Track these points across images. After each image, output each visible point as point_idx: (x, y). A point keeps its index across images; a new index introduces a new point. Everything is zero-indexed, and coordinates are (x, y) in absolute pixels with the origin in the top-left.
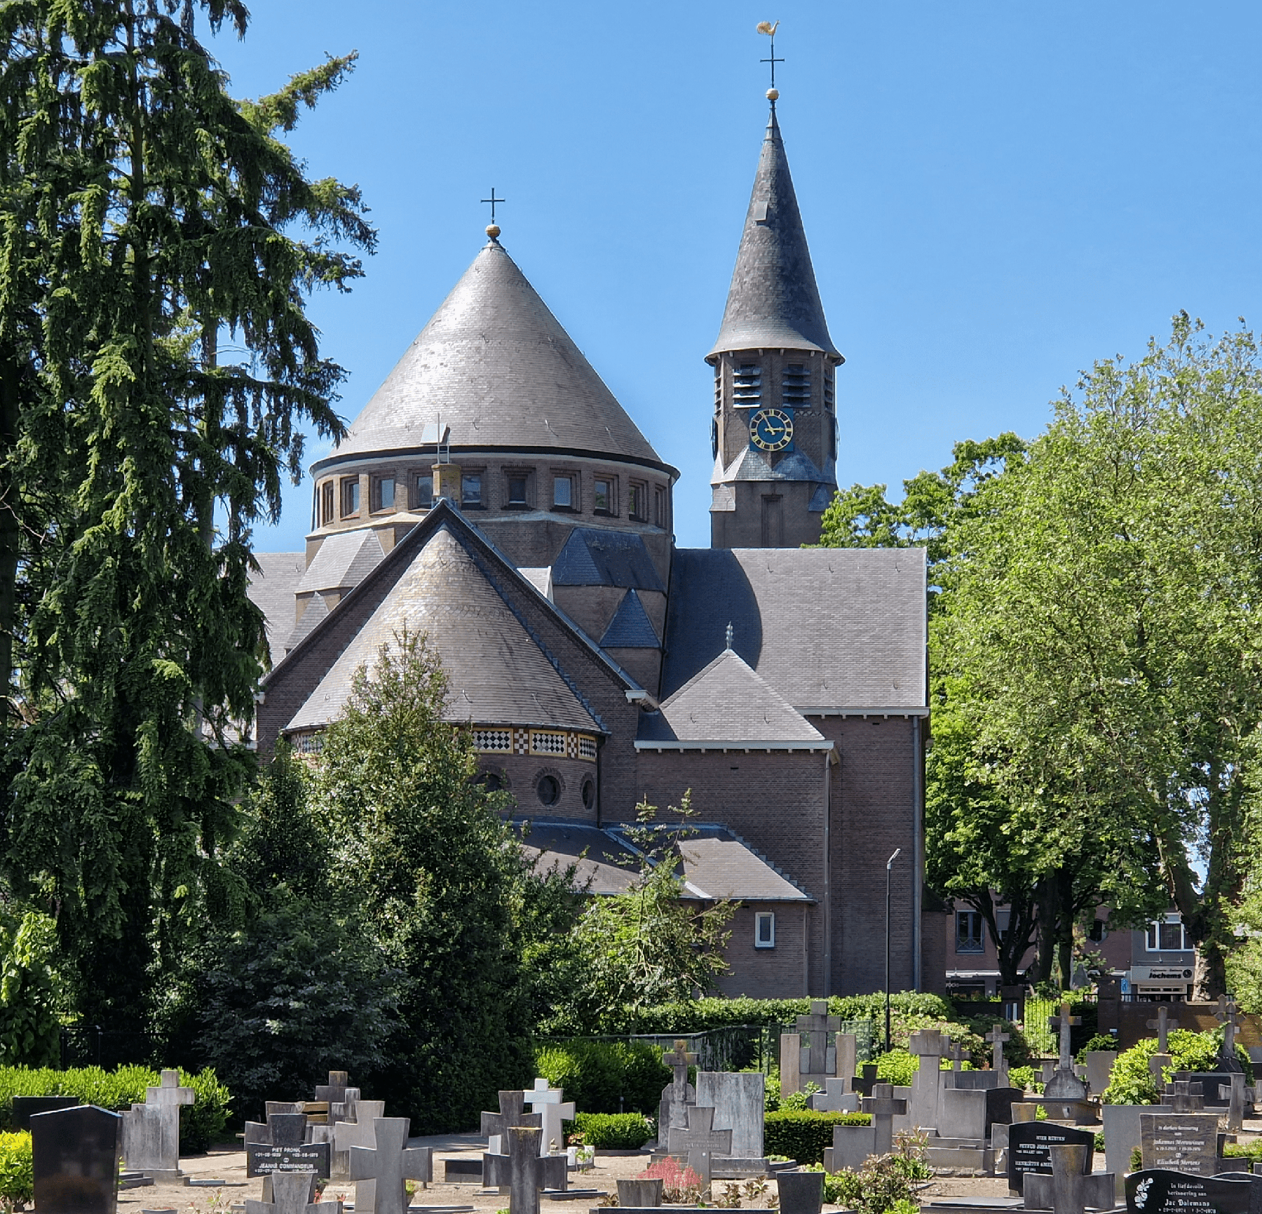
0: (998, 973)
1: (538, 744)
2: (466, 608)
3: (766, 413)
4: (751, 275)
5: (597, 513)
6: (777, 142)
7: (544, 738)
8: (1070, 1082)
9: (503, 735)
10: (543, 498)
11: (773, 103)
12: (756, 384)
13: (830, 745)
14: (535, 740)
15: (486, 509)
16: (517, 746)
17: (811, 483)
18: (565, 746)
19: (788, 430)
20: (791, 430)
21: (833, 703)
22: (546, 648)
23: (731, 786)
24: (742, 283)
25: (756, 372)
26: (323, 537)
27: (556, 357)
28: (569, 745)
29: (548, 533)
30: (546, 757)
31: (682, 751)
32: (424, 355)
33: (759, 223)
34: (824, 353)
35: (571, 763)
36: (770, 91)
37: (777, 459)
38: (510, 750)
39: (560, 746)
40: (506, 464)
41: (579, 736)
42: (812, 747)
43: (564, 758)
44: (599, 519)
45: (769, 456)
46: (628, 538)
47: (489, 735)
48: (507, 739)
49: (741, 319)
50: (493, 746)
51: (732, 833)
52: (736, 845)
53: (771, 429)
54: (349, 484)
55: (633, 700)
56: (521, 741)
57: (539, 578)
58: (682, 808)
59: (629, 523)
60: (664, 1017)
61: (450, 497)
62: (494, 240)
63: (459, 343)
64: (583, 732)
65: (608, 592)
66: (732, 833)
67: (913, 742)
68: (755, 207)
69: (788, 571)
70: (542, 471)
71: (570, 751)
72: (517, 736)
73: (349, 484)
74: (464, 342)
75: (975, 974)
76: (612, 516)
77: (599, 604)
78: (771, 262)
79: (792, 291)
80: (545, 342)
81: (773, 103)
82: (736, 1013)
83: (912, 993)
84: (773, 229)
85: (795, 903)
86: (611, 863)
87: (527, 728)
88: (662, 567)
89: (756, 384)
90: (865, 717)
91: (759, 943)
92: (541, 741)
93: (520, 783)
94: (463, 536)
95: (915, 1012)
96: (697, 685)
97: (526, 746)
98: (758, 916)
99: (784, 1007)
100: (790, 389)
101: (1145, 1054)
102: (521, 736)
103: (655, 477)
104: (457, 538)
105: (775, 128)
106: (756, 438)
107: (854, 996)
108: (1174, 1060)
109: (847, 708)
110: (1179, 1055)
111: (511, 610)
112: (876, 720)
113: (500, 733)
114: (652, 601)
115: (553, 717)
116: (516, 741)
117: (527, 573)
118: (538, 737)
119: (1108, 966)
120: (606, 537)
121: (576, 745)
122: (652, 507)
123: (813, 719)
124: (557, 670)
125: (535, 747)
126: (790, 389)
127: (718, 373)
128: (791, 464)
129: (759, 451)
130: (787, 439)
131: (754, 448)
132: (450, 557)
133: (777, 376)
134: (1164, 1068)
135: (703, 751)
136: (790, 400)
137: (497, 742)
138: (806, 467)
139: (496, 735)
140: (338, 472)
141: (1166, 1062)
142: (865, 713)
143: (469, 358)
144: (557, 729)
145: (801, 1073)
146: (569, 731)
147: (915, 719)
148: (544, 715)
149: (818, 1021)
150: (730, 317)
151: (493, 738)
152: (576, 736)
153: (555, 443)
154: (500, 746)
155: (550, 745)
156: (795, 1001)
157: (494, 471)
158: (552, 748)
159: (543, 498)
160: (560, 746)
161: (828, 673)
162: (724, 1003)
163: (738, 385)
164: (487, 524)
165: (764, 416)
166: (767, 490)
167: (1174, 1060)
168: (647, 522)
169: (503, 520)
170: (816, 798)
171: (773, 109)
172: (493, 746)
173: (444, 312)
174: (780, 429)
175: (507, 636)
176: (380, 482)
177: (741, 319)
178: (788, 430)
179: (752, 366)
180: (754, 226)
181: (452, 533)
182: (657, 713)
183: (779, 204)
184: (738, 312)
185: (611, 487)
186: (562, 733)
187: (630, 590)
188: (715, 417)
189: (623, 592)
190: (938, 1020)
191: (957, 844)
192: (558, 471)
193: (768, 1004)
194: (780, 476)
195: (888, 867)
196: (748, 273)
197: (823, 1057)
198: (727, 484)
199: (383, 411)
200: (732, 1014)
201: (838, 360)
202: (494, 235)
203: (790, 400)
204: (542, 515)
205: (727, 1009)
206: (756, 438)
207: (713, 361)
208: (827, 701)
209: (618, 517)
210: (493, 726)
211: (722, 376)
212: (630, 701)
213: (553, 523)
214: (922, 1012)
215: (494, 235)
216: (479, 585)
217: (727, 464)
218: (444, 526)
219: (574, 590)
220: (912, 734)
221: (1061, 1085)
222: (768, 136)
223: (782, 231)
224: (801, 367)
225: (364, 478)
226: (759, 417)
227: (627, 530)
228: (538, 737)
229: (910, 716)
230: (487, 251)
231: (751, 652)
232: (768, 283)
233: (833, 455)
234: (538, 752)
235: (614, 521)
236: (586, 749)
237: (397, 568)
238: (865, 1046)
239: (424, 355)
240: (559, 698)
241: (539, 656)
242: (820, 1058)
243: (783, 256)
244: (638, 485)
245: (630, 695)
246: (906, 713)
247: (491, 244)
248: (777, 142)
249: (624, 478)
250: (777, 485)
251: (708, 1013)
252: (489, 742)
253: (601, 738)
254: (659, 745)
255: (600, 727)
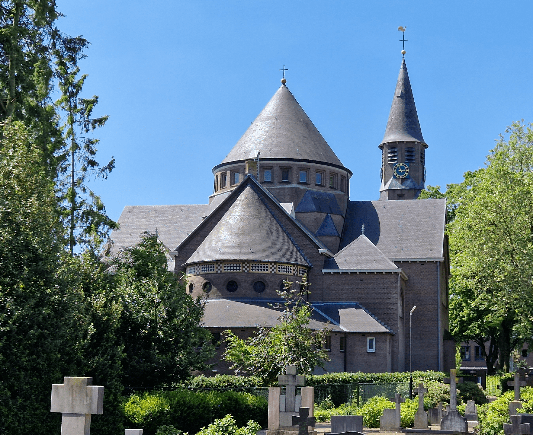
0: (486, 368)
1: (280, 269)
2: (255, 216)
3: (399, 164)
4: (395, 116)
5: (317, 185)
6: (405, 69)
7: (283, 267)
8: (457, 419)
9: (266, 266)
10: (295, 179)
11: (404, 55)
12: (396, 154)
13: (400, 270)
14: (279, 268)
15: (273, 183)
16: (271, 270)
17: (415, 189)
18: (292, 271)
19: (407, 170)
20: (408, 170)
21: (405, 257)
22: (288, 233)
23: (360, 287)
24: (392, 119)
25: (396, 150)
26: (214, 196)
27: (304, 127)
28: (294, 270)
29: (296, 192)
30: (284, 275)
31: (341, 273)
32: (254, 127)
33: (398, 97)
34: (420, 143)
35: (295, 277)
36: (402, 51)
37: (403, 181)
38: (268, 272)
39: (290, 270)
40: (281, 166)
41: (298, 267)
42: (393, 271)
43: (291, 276)
44: (317, 187)
45: (400, 180)
46: (329, 195)
47: (260, 266)
48: (267, 267)
49: (391, 131)
50: (261, 270)
51: (361, 306)
52: (362, 311)
53: (401, 170)
54: (224, 176)
55: (322, 253)
56: (273, 268)
57: (288, 208)
58: (303, 282)
59: (329, 189)
60: (323, 380)
61: (252, 174)
62: (284, 84)
63: (267, 121)
64: (299, 265)
65: (319, 215)
66: (361, 306)
67: (437, 271)
68: (397, 92)
69: (392, 208)
70: (295, 168)
71: (294, 273)
72: (271, 266)
73: (224, 176)
74: (269, 121)
75: (481, 368)
76: (323, 186)
77: (315, 219)
78: (402, 111)
79: (409, 121)
80: (301, 121)
81: (404, 55)
82: (355, 379)
83: (432, 371)
84: (403, 99)
85: (384, 333)
86: (272, 308)
87: (275, 263)
88: (344, 207)
89: (396, 154)
90: (418, 262)
91: (369, 350)
92: (282, 268)
93: (273, 285)
94: (256, 189)
95: (431, 379)
96: (349, 248)
97: (275, 270)
98: (369, 339)
99: (376, 376)
100: (408, 156)
101: (507, 401)
102: (273, 266)
103: (340, 172)
104: (254, 190)
105: (404, 64)
106: (396, 174)
107: (406, 372)
108: (524, 405)
109: (411, 258)
110: (526, 402)
111: (275, 218)
112: (422, 263)
113: (264, 265)
114: (337, 219)
115: (287, 259)
116: (271, 268)
117: (283, 205)
118: (280, 267)
119: (528, 365)
120: (320, 194)
121: (297, 271)
122: (339, 184)
123: (395, 262)
124: (292, 242)
125: (279, 271)
126: (408, 156)
127: (383, 151)
128: (408, 183)
129: (397, 178)
130: (406, 173)
131: (395, 177)
132: (250, 197)
133: (403, 151)
134: (518, 409)
135: (349, 273)
136: (408, 160)
137: (263, 268)
138: (413, 184)
139: (263, 266)
140: (220, 171)
141: (519, 406)
142: (418, 260)
143: (270, 127)
144: (288, 263)
145: (280, 412)
146: (294, 265)
147: (438, 263)
148: (283, 258)
149: (290, 379)
150: (387, 131)
151: (261, 267)
152: (297, 267)
153: (300, 157)
154: (264, 270)
155: (285, 270)
156: (381, 374)
157: (276, 168)
158: (286, 271)
159: (295, 179)
160: (290, 270)
161: (404, 245)
162: (350, 374)
163: (390, 155)
164: (273, 189)
165: (398, 166)
166: (399, 192)
167: (524, 405)
168: (337, 190)
169: (279, 187)
170: (394, 292)
171: (404, 57)
172: (261, 270)
173: (263, 111)
174: (404, 170)
175: (271, 227)
176: (234, 174)
177: (391, 131)
178: (407, 170)
179: (394, 148)
180: (396, 98)
181: (252, 188)
182: (332, 259)
183: (405, 90)
184: (390, 129)
185: (322, 175)
186: (290, 265)
187: (328, 214)
188: (382, 167)
189: (325, 215)
190: (441, 383)
191: (464, 317)
192: (301, 169)
193: (370, 375)
194: (404, 187)
195: (411, 314)
196: (394, 115)
197: (293, 402)
198: (385, 191)
199: (238, 147)
200: (353, 379)
201: (426, 146)
202: (284, 82)
203: (408, 160)
204: (294, 185)
205: (351, 377)
206: (396, 174)
207: (381, 147)
208: (403, 256)
209: (325, 187)
210: (261, 261)
211: (384, 152)
212: (320, 254)
213: (298, 188)
214: (434, 379)
215: (284, 82)
216: (262, 208)
217: (385, 184)
218: (249, 185)
219: (305, 214)
220: (437, 268)
221: (450, 420)
222: (402, 66)
223: (406, 99)
224: (412, 148)
225: (228, 173)
226: (397, 166)
227: (328, 192)
228: (280, 267)
229: (437, 262)
230: (281, 88)
231: (374, 237)
232: (401, 118)
233: (424, 180)
234: (280, 273)
235: (323, 188)
236: (302, 272)
237: (231, 202)
238: (408, 394)
239: (254, 127)
240: (291, 252)
241: (284, 234)
242: (292, 402)
243: (406, 108)
244: (334, 175)
245: (321, 251)
246: (434, 260)
247: (282, 86)
248: (405, 69)
249: (328, 172)
250: (403, 190)
251: (342, 379)
252: (260, 268)
253: (309, 268)
254: (332, 271)
255: (308, 264)
